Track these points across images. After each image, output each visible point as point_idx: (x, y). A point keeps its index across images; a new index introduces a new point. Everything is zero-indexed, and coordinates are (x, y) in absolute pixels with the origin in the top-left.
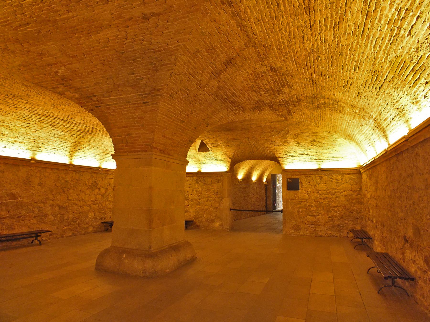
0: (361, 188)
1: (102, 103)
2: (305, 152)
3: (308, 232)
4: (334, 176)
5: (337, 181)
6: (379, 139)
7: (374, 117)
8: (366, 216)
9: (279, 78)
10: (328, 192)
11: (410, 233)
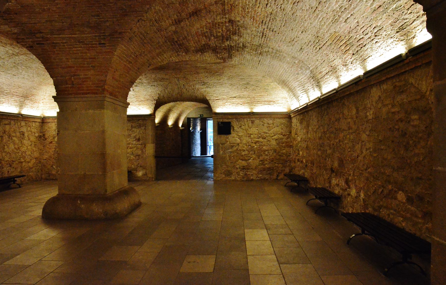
0: (290, 132)
1: (47, 41)
2: (237, 95)
3: (239, 176)
4: (266, 120)
5: (268, 125)
6: (313, 87)
7: (311, 69)
8: (295, 159)
9: (233, 28)
10: (260, 135)
11: (336, 164)
